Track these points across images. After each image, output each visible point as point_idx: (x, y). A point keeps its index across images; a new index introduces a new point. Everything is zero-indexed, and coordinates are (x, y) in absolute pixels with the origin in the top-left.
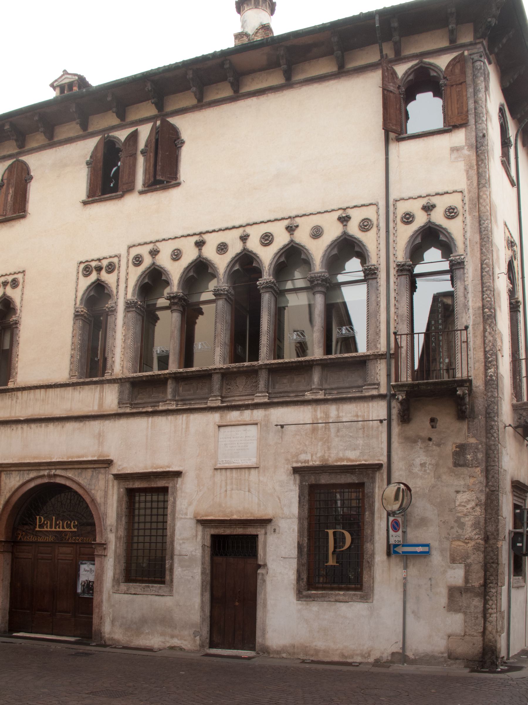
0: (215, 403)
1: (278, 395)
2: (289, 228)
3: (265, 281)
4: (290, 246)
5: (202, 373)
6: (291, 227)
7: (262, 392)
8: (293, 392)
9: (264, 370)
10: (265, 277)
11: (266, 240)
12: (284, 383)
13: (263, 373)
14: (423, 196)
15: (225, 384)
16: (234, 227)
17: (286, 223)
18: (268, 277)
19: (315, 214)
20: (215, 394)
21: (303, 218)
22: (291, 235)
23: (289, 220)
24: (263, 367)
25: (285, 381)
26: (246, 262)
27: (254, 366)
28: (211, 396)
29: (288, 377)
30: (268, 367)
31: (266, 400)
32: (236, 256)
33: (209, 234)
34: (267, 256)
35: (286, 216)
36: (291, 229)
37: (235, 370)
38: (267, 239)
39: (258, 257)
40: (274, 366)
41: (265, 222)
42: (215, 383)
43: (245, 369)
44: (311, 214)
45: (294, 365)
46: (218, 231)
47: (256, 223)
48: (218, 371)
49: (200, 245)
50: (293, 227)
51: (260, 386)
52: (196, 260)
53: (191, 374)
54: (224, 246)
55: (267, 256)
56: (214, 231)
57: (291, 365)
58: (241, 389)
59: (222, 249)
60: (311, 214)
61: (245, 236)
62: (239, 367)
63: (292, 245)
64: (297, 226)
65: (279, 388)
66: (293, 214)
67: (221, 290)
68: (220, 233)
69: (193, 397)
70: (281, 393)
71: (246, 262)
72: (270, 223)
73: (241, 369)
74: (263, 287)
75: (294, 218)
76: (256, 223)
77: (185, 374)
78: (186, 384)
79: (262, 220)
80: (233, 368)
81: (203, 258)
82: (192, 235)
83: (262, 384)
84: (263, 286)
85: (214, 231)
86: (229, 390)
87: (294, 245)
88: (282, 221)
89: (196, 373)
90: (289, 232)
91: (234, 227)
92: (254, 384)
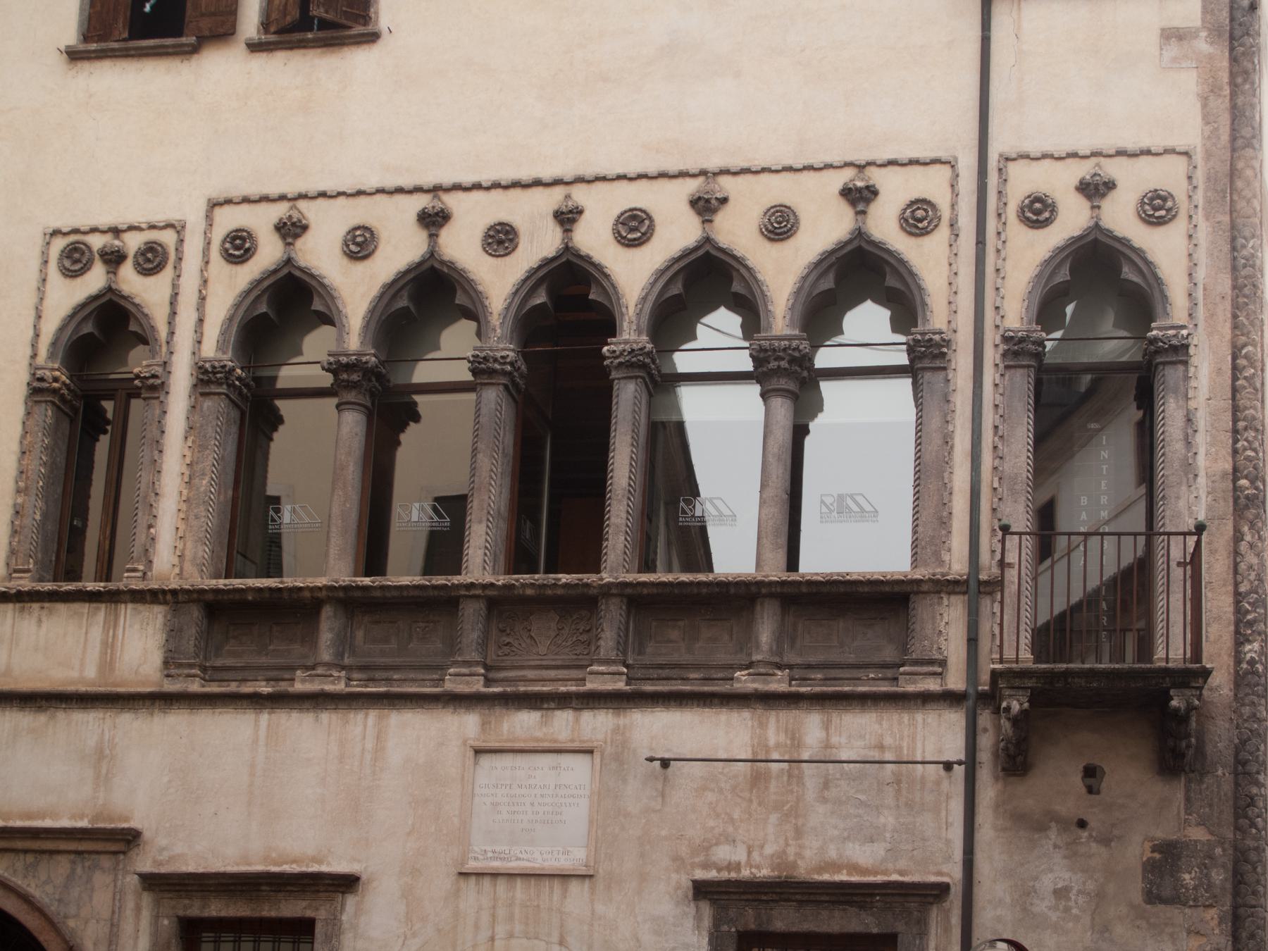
0: (468, 683)
2: (701, 203)
3: (628, 347)
4: (701, 252)
6: (708, 201)
7: (607, 662)
10: (625, 336)
11: (632, 230)
13: (612, 608)
16: (537, 183)
20: (468, 658)
21: (741, 179)
22: (703, 222)
23: (701, 179)
24: (614, 591)
25: (674, 634)
27: (587, 585)
28: (455, 664)
29: (681, 623)
30: (629, 591)
31: (621, 685)
32: (540, 267)
33: (460, 195)
35: (694, 169)
37: (529, 592)
38: (633, 229)
39: (607, 276)
40: (645, 591)
41: (631, 179)
43: (560, 592)
45: (705, 591)
46: (488, 189)
47: (604, 179)
49: (434, 224)
50: (713, 201)
51: (602, 643)
53: (395, 593)
54: (507, 233)
56: (477, 186)
57: (695, 591)
59: (500, 242)
61: (571, 212)
64: (724, 201)
65: (655, 653)
66: (713, 164)
67: (495, 360)
69: (398, 661)
70: (661, 667)
72: (644, 182)
73: (549, 592)
74: (620, 364)
75: (715, 174)
77: (378, 594)
80: (524, 586)
81: (443, 262)
82: (410, 192)
83: (608, 640)
84: (621, 360)
85: (477, 186)
87: (713, 252)
88: (680, 181)
90: (699, 213)
91: (537, 183)
92: (584, 637)
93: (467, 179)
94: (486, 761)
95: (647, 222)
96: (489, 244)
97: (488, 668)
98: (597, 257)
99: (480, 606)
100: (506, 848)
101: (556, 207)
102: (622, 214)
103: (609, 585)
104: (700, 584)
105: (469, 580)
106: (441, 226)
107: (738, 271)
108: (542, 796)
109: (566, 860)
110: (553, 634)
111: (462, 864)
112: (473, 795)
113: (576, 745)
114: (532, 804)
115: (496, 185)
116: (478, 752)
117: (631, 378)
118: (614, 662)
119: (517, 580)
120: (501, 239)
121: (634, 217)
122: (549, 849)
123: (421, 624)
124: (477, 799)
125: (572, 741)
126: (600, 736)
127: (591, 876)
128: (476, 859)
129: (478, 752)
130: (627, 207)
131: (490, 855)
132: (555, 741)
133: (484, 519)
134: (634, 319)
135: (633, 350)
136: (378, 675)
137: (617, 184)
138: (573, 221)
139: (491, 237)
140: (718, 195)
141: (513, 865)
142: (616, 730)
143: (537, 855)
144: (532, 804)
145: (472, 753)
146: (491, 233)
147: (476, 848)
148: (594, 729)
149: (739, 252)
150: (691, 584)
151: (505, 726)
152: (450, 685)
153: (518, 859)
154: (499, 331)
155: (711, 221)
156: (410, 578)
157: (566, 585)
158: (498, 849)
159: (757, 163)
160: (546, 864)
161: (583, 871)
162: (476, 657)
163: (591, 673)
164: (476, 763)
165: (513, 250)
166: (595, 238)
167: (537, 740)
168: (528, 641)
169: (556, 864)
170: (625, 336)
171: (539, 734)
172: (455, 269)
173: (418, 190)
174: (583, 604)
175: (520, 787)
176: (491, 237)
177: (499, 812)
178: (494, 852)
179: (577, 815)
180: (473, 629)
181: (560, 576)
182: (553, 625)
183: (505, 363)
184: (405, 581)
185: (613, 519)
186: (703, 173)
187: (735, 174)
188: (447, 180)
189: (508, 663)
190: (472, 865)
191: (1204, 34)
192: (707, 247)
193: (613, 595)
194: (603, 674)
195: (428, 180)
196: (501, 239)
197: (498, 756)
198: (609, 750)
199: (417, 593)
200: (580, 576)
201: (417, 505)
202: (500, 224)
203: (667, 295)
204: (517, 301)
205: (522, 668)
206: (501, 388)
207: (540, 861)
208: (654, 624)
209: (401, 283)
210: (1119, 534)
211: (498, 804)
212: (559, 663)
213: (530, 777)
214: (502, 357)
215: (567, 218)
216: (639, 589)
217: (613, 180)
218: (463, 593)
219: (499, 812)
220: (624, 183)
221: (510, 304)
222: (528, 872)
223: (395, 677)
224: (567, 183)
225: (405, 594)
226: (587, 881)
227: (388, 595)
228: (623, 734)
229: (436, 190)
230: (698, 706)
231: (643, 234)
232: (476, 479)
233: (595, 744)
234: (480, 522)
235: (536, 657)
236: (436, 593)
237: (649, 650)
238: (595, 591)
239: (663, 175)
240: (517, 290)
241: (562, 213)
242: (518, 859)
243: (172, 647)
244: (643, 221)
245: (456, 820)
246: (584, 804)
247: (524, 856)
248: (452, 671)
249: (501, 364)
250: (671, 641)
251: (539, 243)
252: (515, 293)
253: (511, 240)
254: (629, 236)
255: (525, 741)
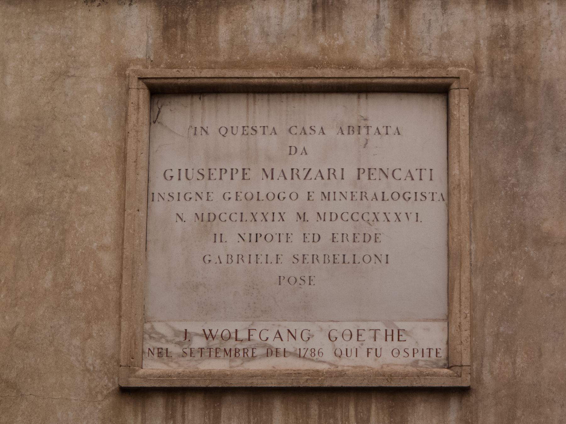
94: (178, 116)
100: (239, 326)
108: (326, 196)
109: (395, 353)
111: (132, 365)
112: (149, 197)
113: (403, 73)
114: (302, 217)
116: (161, 91)
122: (352, 326)
124: (158, 207)
125: (392, 64)
126: (462, 54)
127: (463, 391)
128: (162, 354)
129: (161, 91)
131: (198, 343)
132: (352, 65)
141: (259, 367)
142: (500, 38)
143: (319, 341)
144: (302, 217)
145: (144, 94)
147: (161, 328)
148: (446, 36)
151: (223, 31)
153: (272, 352)
158: (218, 327)
160: (345, 364)
161: (444, 378)
164: (153, 120)
167: (306, 63)
169: (372, 363)
171: (308, 49)
175: (270, 175)
177: (219, 238)
178: (208, 336)
179: (416, 244)
190: (153, 369)
191: (320, 58)
197: (209, 102)
198: (486, 86)
207: (328, 356)
210: (358, 335)
211: (214, 218)
213: (292, 151)
219: (219, 238)
222: (302, 383)
226: (454, 404)
228: (518, 47)
233: (453, 71)
242: (272, 352)
245: (108, 260)
246: (434, 213)
247: (289, 345)
255: (273, 65)
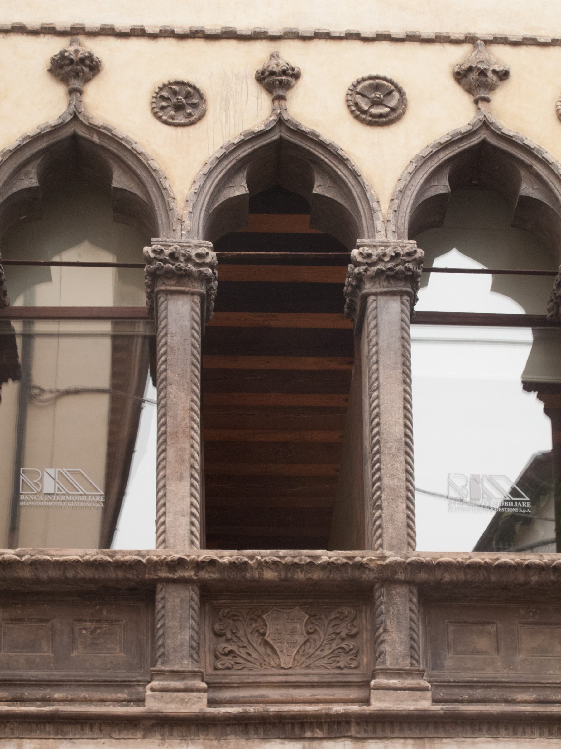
0: (182, 701)
1: (479, 693)
2: (474, 76)
3: (390, 251)
4: (475, 141)
5: (112, 574)
6: (483, 73)
7: (398, 673)
8: (525, 686)
9: (403, 590)
10: (380, 238)
11: (376, 103)
12: (476, 652)
13: (397, 599)
14: (149, 30)
15: (208, 635)
16: (229, 35)
17: (458, 55)
18: (392, 239)
19: (340, 38)
20: (177, 668)
21: (523, 51)
22: (476, 102)
23: (467, 48)
24: (401, 576)
25: (483, 643)
26: (283, 177)
27: (361, 566)
28: (160, 673)
29: (491, 628)
30: (423, 576)
31: (424, 704)
32: (242, 144)
33: (112, 42)
34: (385, 166)
35: (457, 32)
36: (277, 81)
37: (269, 575)
38: (377, 102)
39: (343, 161)
40: (447, 577)
41: (366, 40)
42: (172, 623)
43: (316, 575)
44: (318, 36)
45: (535, 579)
46: (154, 36)
47: (328, 36)
48: (189, 574)
49: (77, 75)
50: (490, 74)
51: (386, 647)
52: (56, 128)
53: (54, 574)
54: (188, 96)
55: (385, 166)
56: (139, 33)
57: (521, 578)
58: (286, 660)
59: (179, 107)
60: (318, 36)
61: (284, 72)
62: (295, 566)
63: (484, 143)
64: (504, 75)
65: (453, 666)
66: (484, 29)
67: (188, 259)
68: (167, 45)
69: (57, 675)
70: (470, 685)
71: (283, 177)
72: (385, 45)
73: (300, 576)
74: (380, 273)
75: (487, 42)
76: (328, 36)
77: (26, 574)
78: (20, 620)
79: (353, 28)
80: (262, 565)
81: (93, 128)
82: (35, 33)
83: (395, 643)
84: (381, 266)
85: (139, 33)
86: (228, 661)
87: (493, 141)
88: (436, 48)
89: (82, 574)
90: (469, 91)
91: (229, 35)
92: (350, 644)
93: (123, 23)
95: (396, 94)
96: (163, 108)
97: (212, 686)
98: (327, 135)
99: (191, 595)
101: (260, 68)
102: (359, 82)
103: (395, 567)
104: (529, 567)
105: (176, 556)
106: (87, 80)
107: (529, 168)
110: (300, 639)
115: (167, 34)
117: (393, 294)
118: (409, 673)
119: (252, 557)
120: (179, 103)
121: (377, 88)
123: (88, 624)
130: (366, 74)
133: (187, 475)
134: (391, 217)
135: (397, 255)
136: (27, 693)
137: (345, 44)
138: (287, 86)
139: (163, 98)
140: (497, 68)
146: (165, 94)
149: (532, 141)
150: (517, 567)
152: (154, 704)
154: (187, 222)
155: (487, 100)
156: (81, 552)
157: (330, 566)
159: (543, 33)
162: (187, 665)
163: (378, 688)
165: (200, 119)
166: (320, 108)
168: (262, 649)
170: (380, 238)
172: (114, 139)
173: (48, 30)
174: (350, 597)
176: (163, 98)
180: (182, 627)
181: (319, 552)
182: (300, 627)
183: (203, 264)
184: (73, 554)
185: (386, 480)
186: (470, 39)
187: (515, 44)
188: (93, 22)
189: (234, 679)
192: (484, 135)
193: (400, 582)
194: (396, 689)
195: (63, 20)
196: (179, 103)
199: (90, 574)
200: (349, 553)
201: (52, 471)
202: (177, 83)
203: (423, 199)
204: (210, 186)
205: (257, 685)
206: (197, 299)
208: (451, 628)
209: (29, 153)
212: (315, 679)
214: (199, 255)
215: (277, 81)
216: (438, 574)
217: (340, 38)
218: (164, 574)
220: (357, 45)
221: (202, 187)
223: (57, 696)
224: (273, 38)
225: (70, 574)
227: (43, 575)
229: (75, 32)
230: (541, 735)
231: (393, 110)
232: (170, 421)
234: (181, 478)
235: (275, 671)
236: (120, 574)
237: (448, 663)
238: (372, 576)
239: (412, 38)
240: (211, 171)
241: (272, 73)
243: (466, 87)
244: (390, 93)
248: (155, 684)
249: (196, 265)
250: (479, 652)
251: (238, 112)
252: (208, 175)
253: (195, 106)
254: (374, 111)
